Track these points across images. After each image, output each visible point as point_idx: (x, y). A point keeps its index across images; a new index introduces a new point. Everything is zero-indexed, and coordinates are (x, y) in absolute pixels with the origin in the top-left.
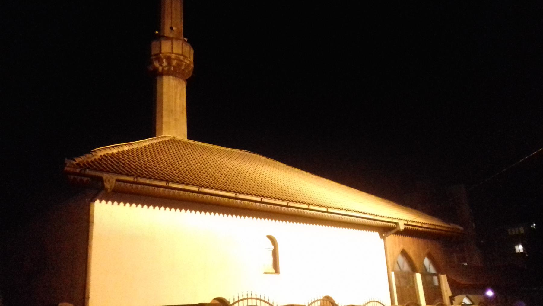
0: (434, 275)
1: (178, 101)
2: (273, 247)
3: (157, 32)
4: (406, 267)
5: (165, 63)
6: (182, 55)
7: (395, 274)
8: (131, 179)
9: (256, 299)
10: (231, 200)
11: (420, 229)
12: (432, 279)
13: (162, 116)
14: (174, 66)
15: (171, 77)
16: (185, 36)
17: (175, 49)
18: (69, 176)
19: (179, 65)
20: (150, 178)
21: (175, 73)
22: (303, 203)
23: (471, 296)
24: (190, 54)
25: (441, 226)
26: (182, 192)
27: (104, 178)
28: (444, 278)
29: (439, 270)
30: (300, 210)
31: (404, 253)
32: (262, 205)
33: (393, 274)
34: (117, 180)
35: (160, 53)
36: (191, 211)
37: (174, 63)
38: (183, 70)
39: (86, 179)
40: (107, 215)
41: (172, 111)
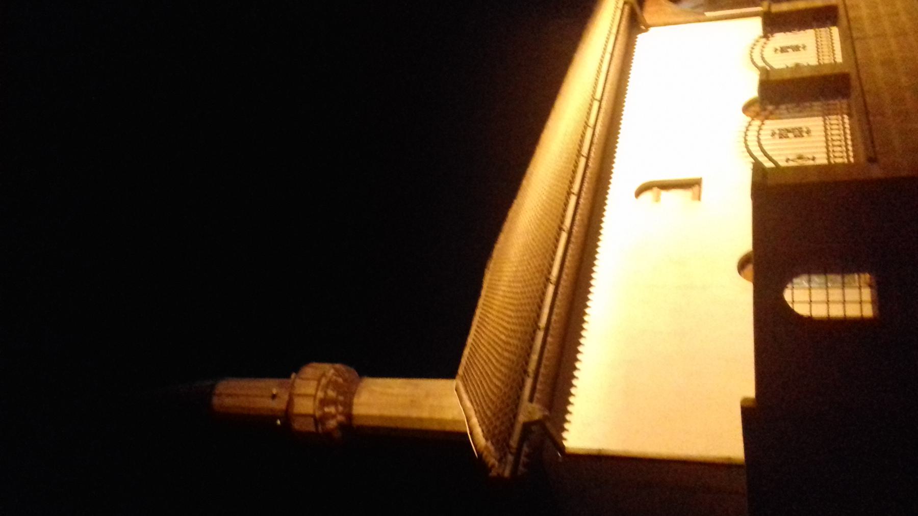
1: (396, 391)
3: (279, 422)
5: (331, 410)
6: (319, 381)
8: (529, 383)
15: (355, 400)
17: (309, 392)
18: (519, 473)
21: (348, 394)
26: (556, 310)
27: (526, 419)
32: (583, 194)
33: (709, 14)
34: (531, 400)
35: (313, 416)
37: (331, 393)
38: (345, 380)
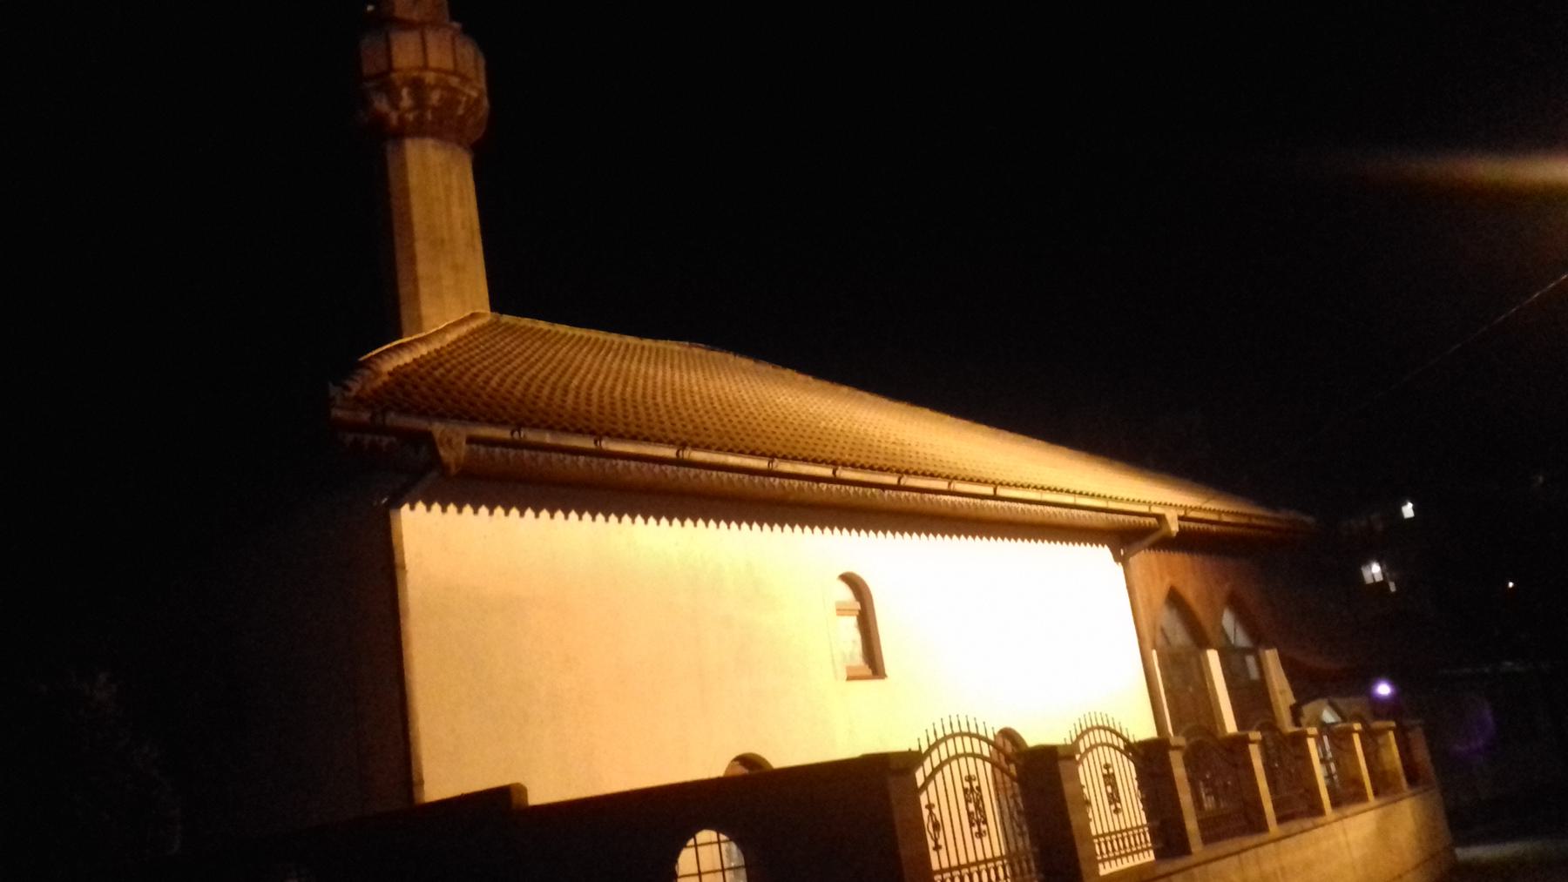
0: (1245, 651)
1: (456, 210)
2: (858, 606)
4: (1180, 637)
5: (406, 101)
6: (455, 73)
7: (1159, 655)
9: (970, 735)
10: (757, 479)
11: (1214, 528)
12: (1244, 662)
13: (412, 260)
14: (435, 109)
15: (430, 142)
16: (454, 18)
17: (433, 57)
19: (450, 102)
20: (551, 428)
21: (440, 127)
22: (932, 476)
23: (1337, 701)
24: (476, 67)
25: (1250, 516)
27: (437, 435)
28: (1271, 657)
29: (1259, 640)
30: (927, 496)
31: (1175, 599)
34: (471, 440)
35: (391, 69)
36: (658, 520)
37: (435, 97)
39: (386, 440)
40: (439, 544)
41: (443, 241)
